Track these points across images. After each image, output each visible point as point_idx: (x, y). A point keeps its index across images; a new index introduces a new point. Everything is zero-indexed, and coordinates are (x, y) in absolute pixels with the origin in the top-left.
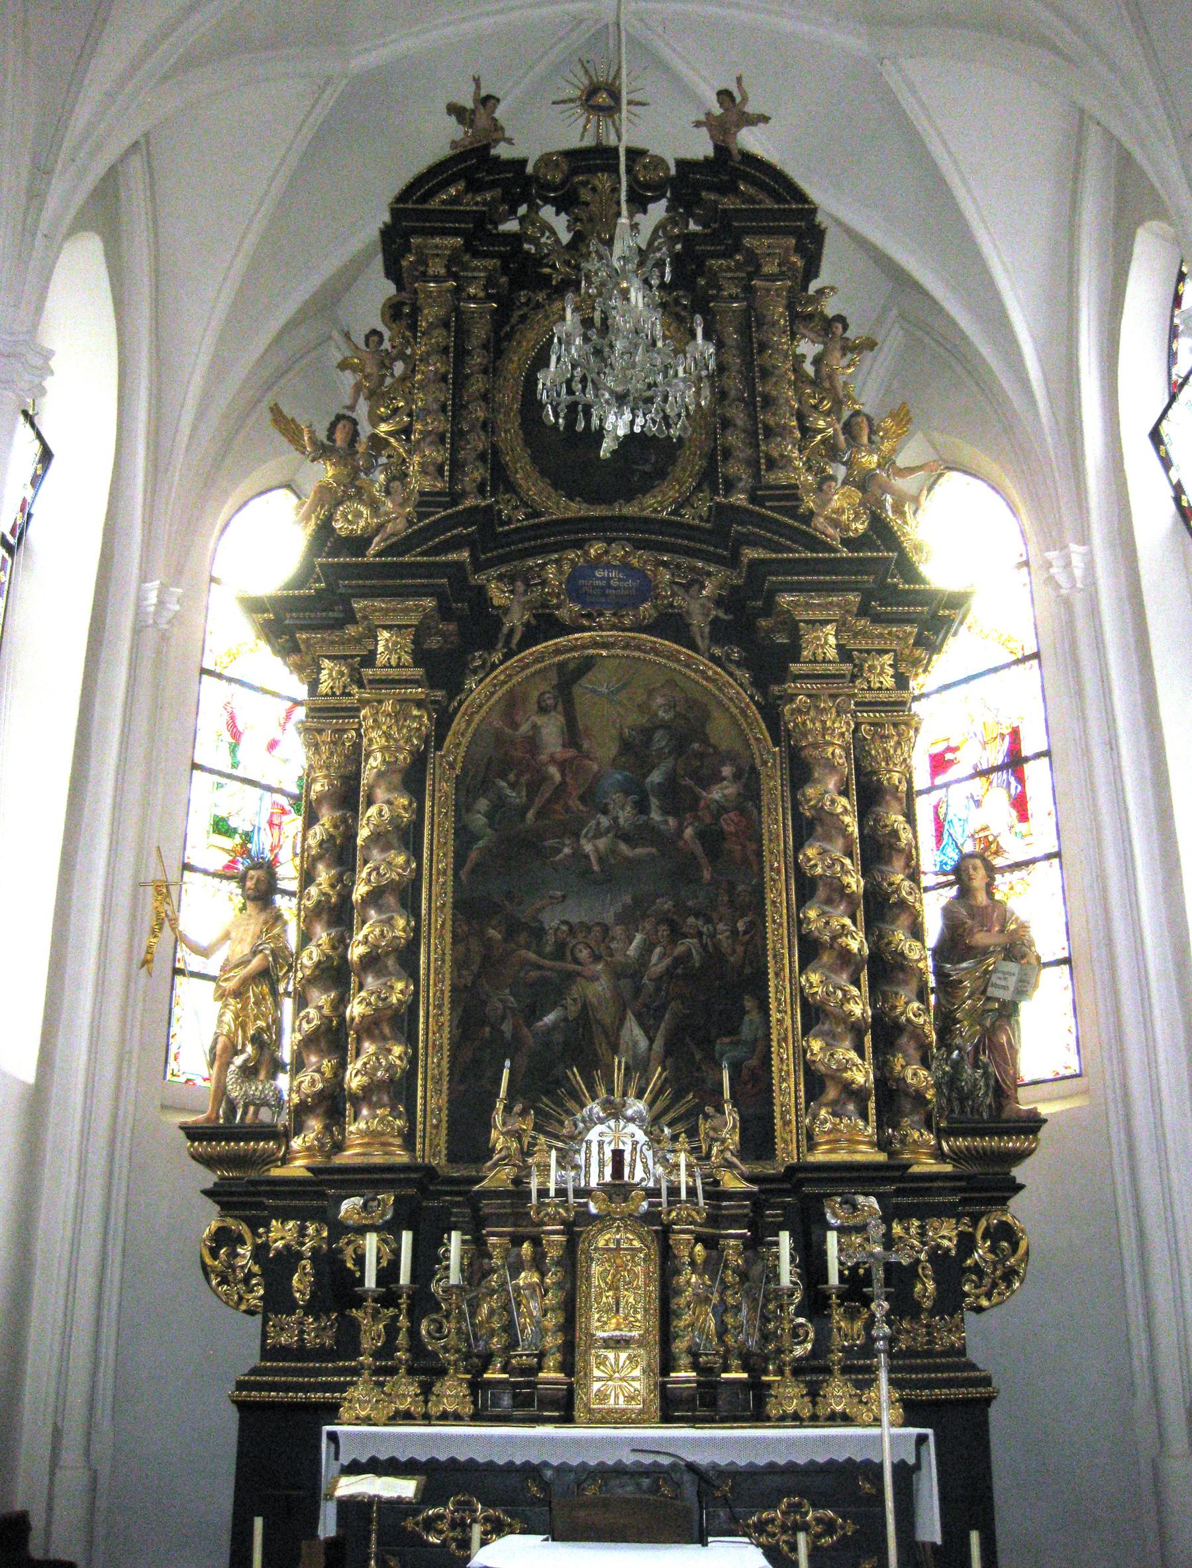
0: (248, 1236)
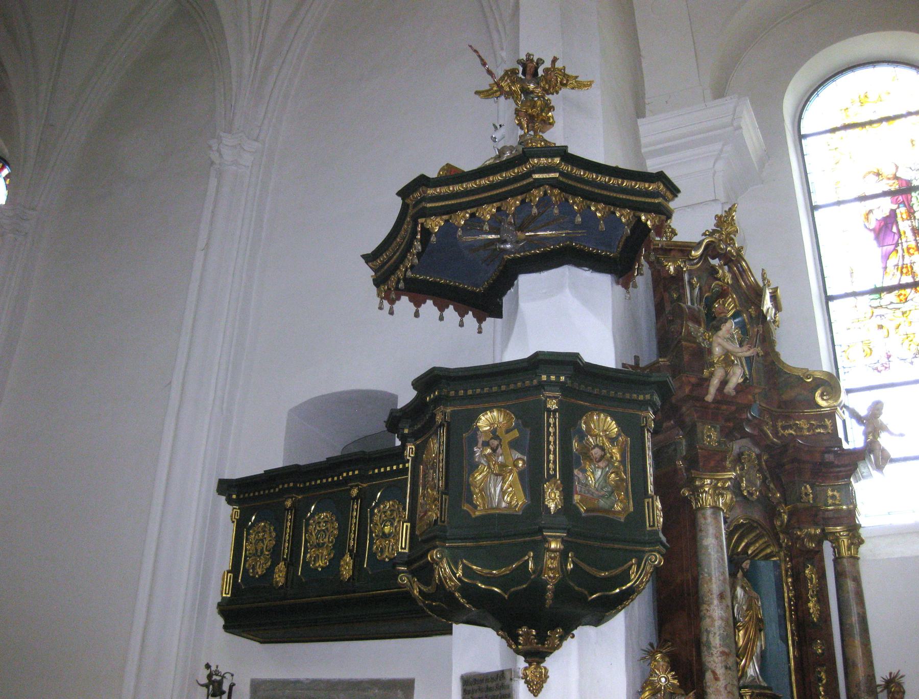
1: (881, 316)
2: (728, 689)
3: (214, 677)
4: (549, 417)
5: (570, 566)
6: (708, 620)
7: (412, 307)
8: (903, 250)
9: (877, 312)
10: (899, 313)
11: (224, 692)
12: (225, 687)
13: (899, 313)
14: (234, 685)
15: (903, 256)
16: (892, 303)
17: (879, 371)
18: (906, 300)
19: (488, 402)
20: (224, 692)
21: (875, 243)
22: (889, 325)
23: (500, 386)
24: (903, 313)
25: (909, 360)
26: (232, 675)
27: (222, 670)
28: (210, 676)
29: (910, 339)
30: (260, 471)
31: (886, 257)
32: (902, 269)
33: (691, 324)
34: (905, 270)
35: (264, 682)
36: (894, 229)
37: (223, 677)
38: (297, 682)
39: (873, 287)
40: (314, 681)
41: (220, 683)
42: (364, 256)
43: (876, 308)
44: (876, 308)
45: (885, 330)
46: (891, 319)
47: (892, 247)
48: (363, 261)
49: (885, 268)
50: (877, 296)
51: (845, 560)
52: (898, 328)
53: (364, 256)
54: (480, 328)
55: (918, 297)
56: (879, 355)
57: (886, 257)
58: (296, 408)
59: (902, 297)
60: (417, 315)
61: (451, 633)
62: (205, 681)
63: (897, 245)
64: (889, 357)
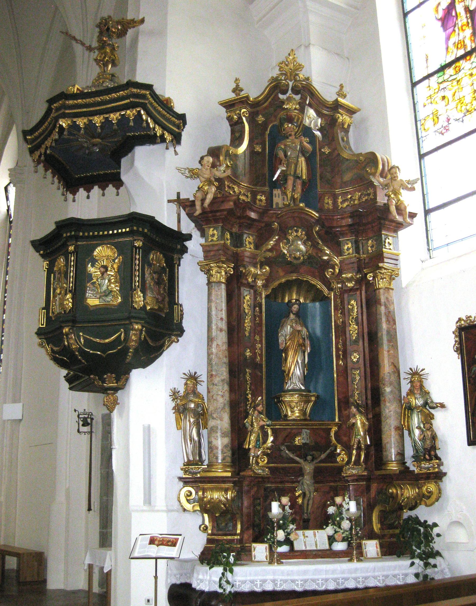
0: (196, 234)
1: (444, 89)
3: (81, 416)
4: (71, 257)
5: (266, 427)
6: (387, 427)
7: (114, 190)
8: (459, 29)
9: (442, 86)
10: (455, 82)
13: (455, 82)
15: (459, 34)
16: (451, 76)
17: (443, 134)
18: (460, 71)
19: (103, 240)
21: (441, 29)
22: (448, 94)
24: (458, 81)
25: (461, 120)
29: (461, 102)
31: (448, 38)
32: (458, 45)
33: (285, 169)
34: (459, 46)
36: (454, 14)
39: (439, 67)
43: (441, 83)
44: (441, 83)
45: (446, 99)
46: (451, 88)
47: (452, 29)
49: (447, 48)
50: (441, 74)
51: (381, 291)
52: (454, 95)
54: (175, 151)
55: (475, 59)
56: (442, 121)
57: (448, 38)
59: (457, 69)
60: (118, 194)
61: (185, 114)
63: (455, 26)
64: (448, 120)
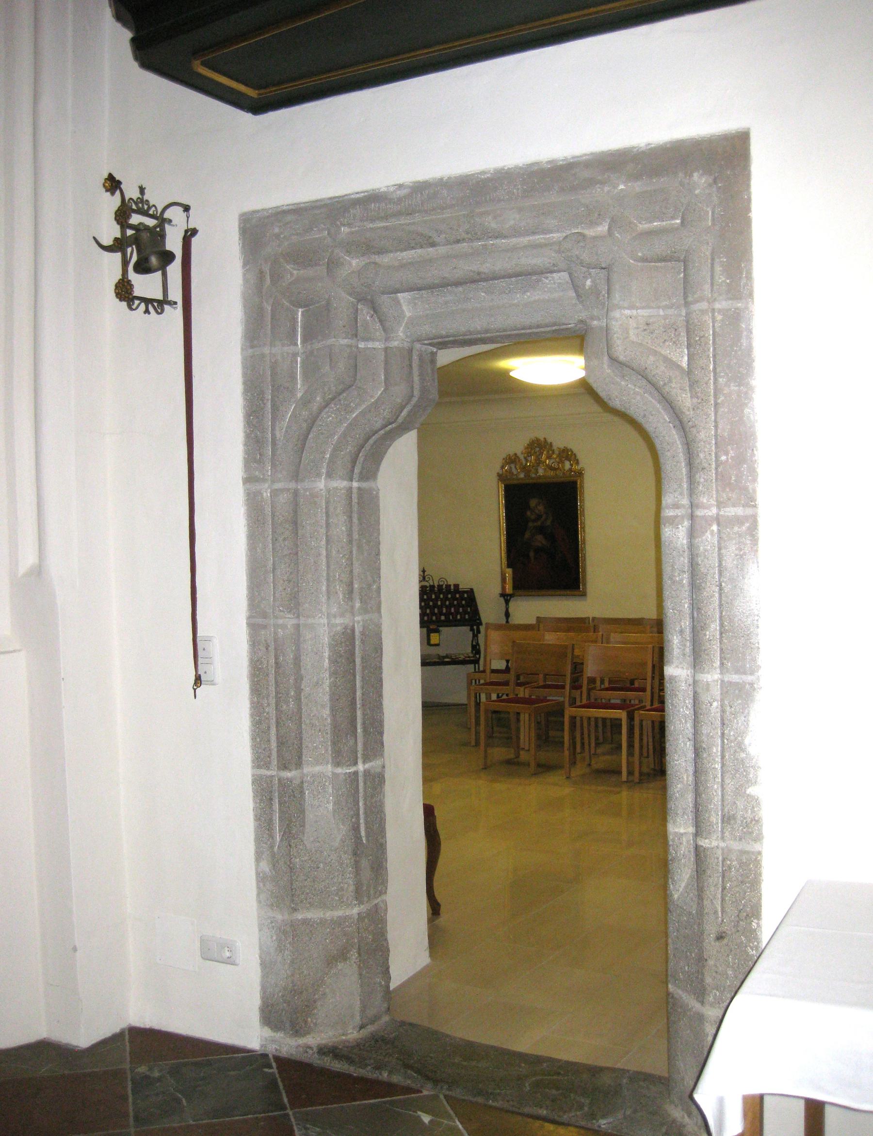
2: (747, 686)
3: (135, 219)
11: (168, 257)
12: (173, 243)
14: (194, 232)
20: (168, 257)
23: (151, 1069)
26: (187, 208)
27: (157, 199)
28: (122, 215)
30: (110, 1035)
35: (279, 214)
37: (163, 221)
38: (373, 198)
40: (420, 187)
41: (158, 235)
42: (110, 175)
48: (106, 176)
53: (110, 175)
58: (757, 863)
62: (110, 232)
